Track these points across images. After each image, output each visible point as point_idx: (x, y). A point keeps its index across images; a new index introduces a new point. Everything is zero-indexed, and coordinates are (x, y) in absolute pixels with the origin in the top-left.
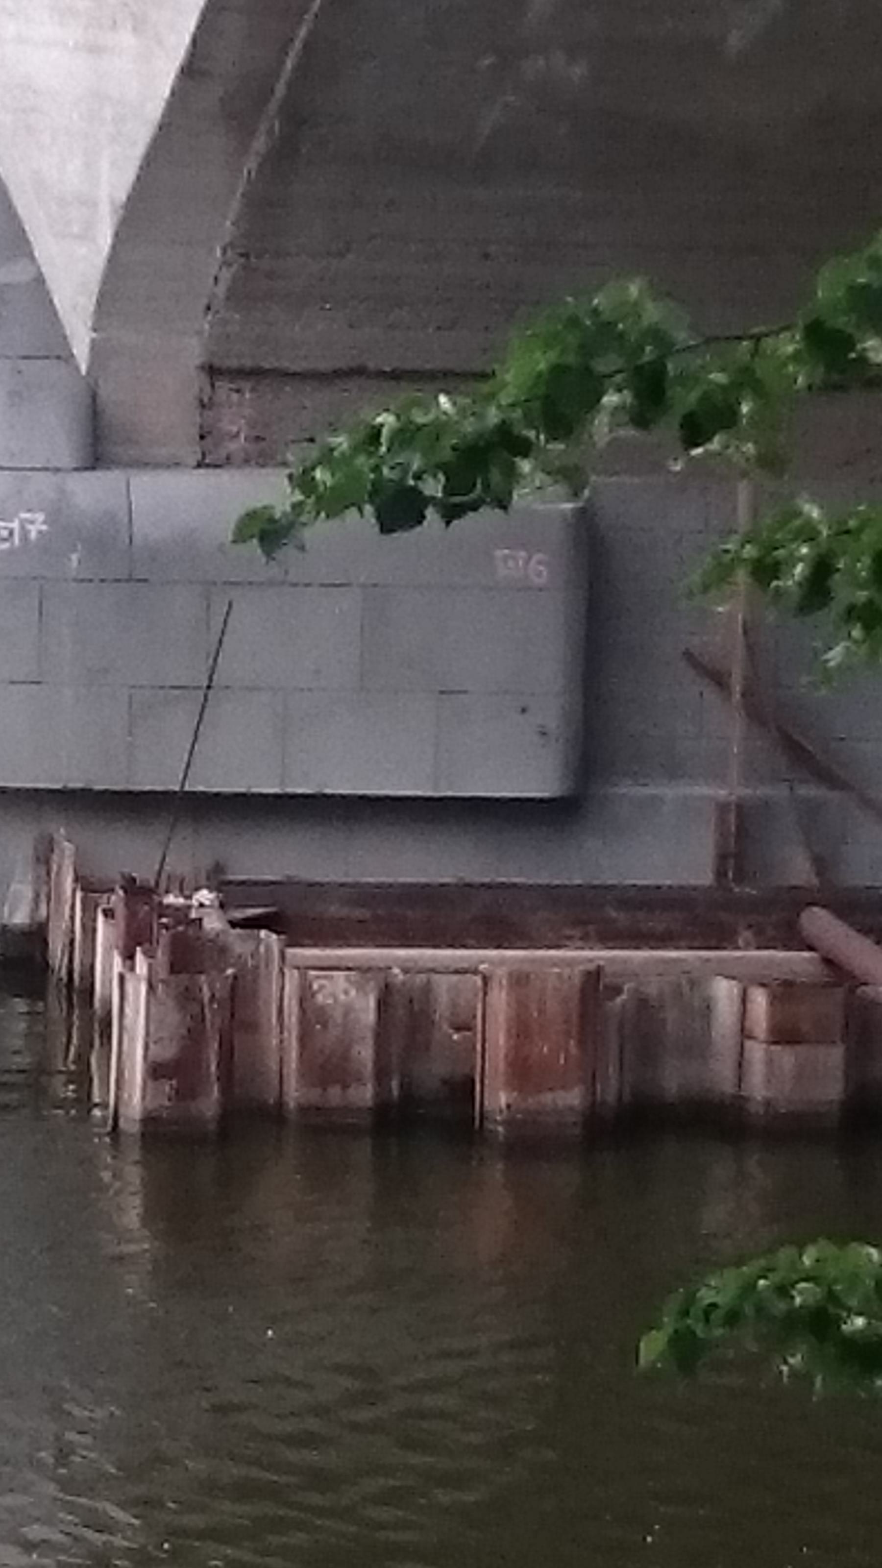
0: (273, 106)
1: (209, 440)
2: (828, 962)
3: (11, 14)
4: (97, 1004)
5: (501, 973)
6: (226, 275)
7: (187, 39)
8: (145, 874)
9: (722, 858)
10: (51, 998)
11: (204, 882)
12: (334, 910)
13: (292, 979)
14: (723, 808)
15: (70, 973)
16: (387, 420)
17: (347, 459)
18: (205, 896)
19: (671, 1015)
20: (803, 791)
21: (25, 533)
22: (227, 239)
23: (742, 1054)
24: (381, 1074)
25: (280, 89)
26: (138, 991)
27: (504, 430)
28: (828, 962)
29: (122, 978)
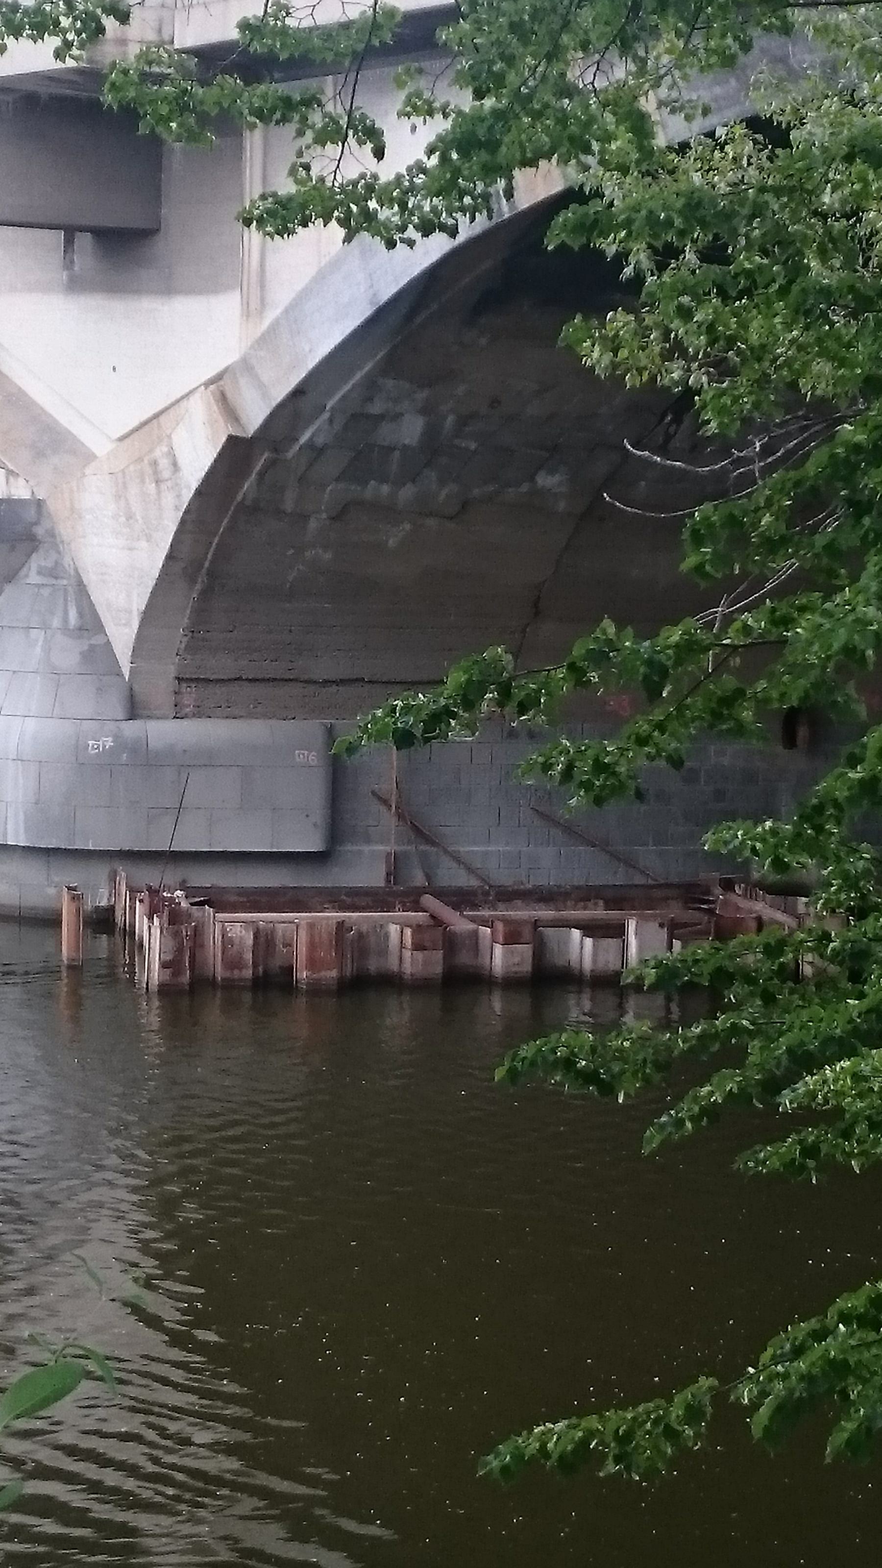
0: (204, 571)
1: (178, 707)
2: (432, 917)
3: (95, 535)
4: (137, 938)
5: (303, 923)
6: (185, 639)
7: (168, 546)
8: (155, 884)
9: (388, 874)
10: (117, 934)
11: (178, 888)
12: (233, 898)
13: (218, 926)
14: (389, 854)
15: (125, 925)
16: (399, 703)
17: (382, 719)
18: (179, 893)
19: (372, 939)
20: (422, 847)
21: (104, 746)
22: (185, 626)
23: (401, 955)
24: (255, 965)
25: (207, 565)
26: (156, 932)
27: (446, 707)
28: (432, 917)
29: (150, 927)
